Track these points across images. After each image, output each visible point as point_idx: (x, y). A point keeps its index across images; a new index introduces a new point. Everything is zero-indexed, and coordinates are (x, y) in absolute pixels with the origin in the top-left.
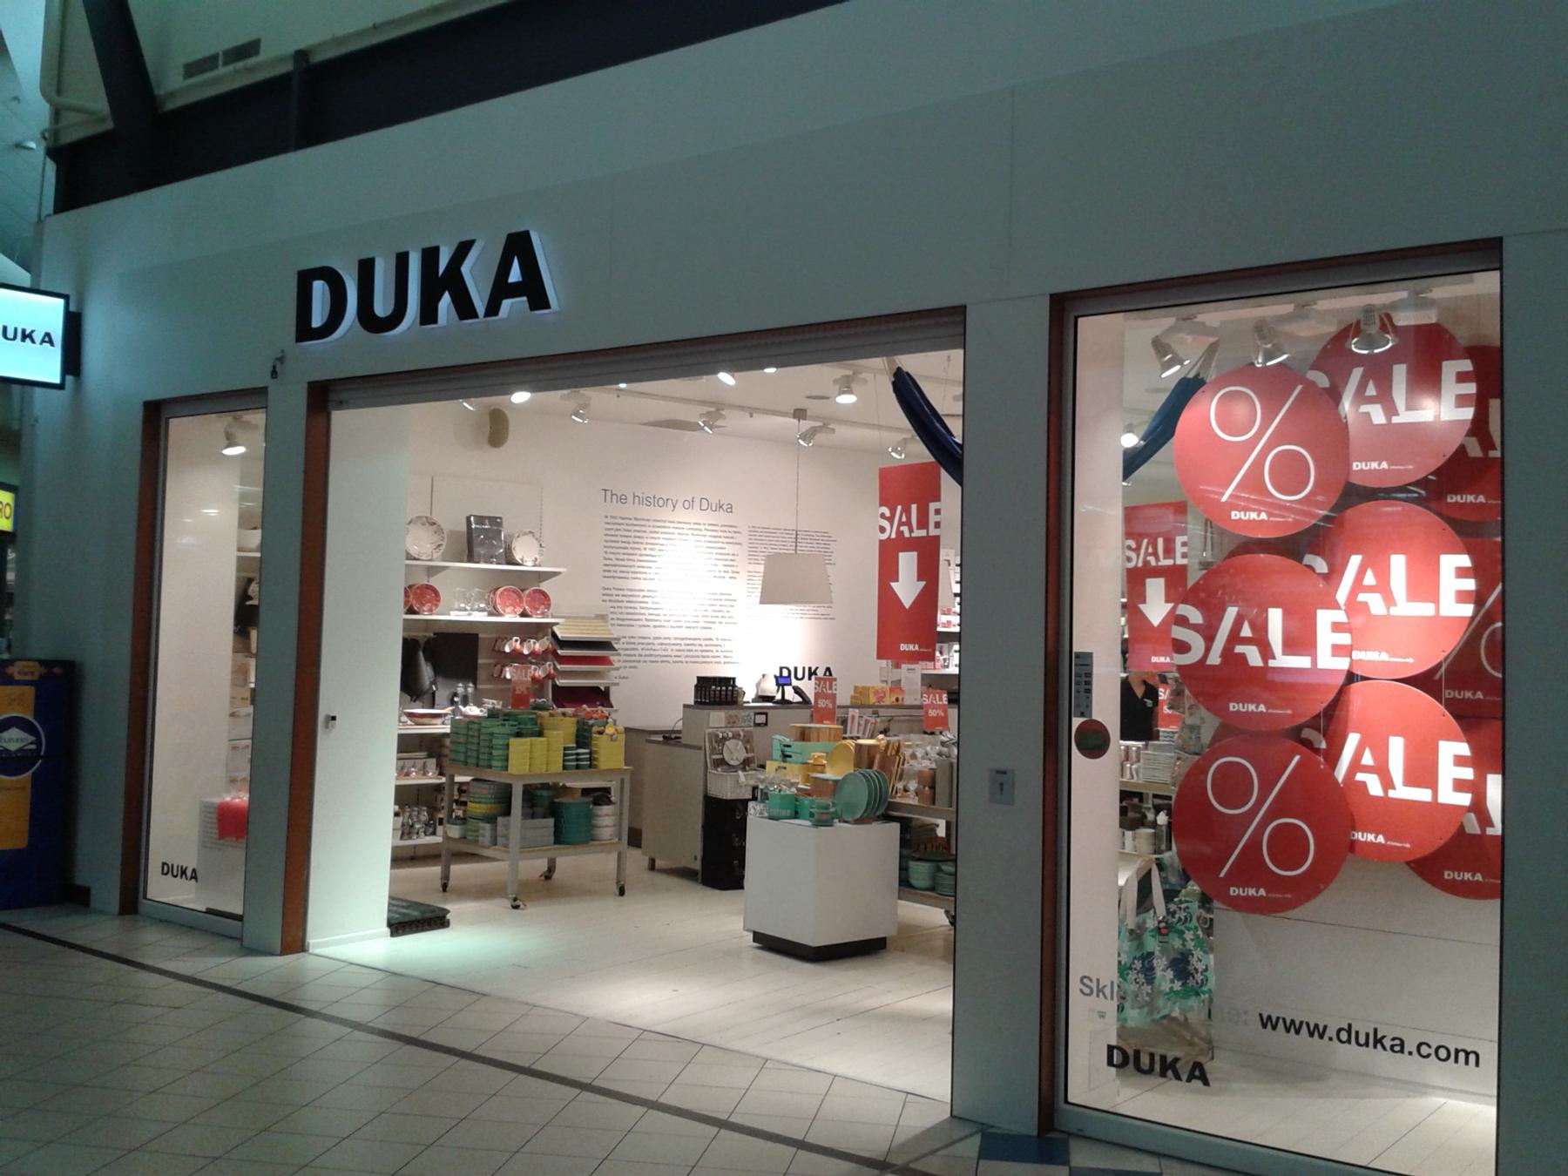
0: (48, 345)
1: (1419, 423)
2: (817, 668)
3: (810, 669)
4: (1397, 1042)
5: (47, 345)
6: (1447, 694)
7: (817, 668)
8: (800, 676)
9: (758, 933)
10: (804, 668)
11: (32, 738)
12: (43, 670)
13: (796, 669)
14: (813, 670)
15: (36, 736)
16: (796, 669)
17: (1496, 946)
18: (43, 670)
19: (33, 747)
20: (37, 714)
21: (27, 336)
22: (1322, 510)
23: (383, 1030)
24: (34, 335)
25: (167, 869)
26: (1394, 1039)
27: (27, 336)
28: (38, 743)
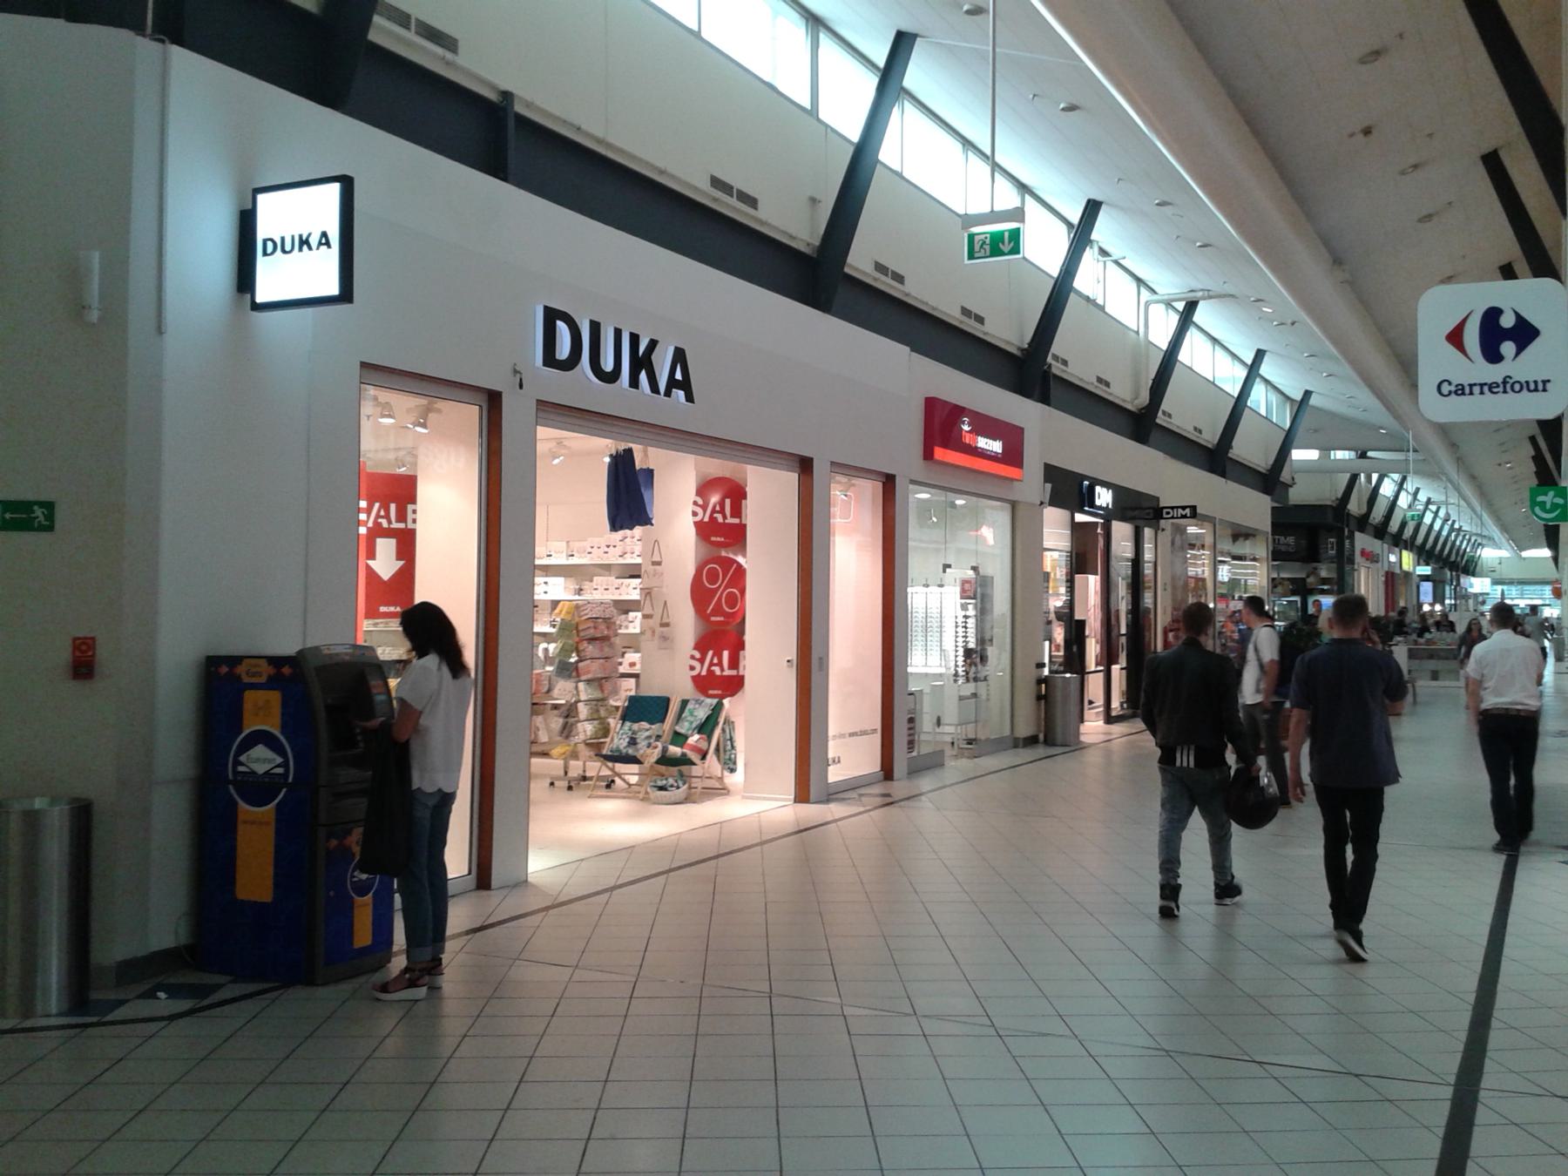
0: (325, 247)
1: (909, 59)
2: (310, 235)
3: (301, 236)
4: (1460, 387)
5: (324, 248)
6: (1206, 572)
7: (310, 235)
8: (288, 248)
9: (1049, 465)
10: (293, 237)
11: (279, 760)
12: (271, 670)
13: (283, 239)
14: (304, 238)
15: (283, 758)
16: (283, 239)
17: (1482, 582)
18: (271, 670)
19: (280, 770)
20: (284, 728)
21: (304, 242)
22: (1345, 817)
23: (467, 931)
24: (311, 240)
25: (1164, 413)
26: (1457, 386)
27: (304, 242)
28: (285, 765)
